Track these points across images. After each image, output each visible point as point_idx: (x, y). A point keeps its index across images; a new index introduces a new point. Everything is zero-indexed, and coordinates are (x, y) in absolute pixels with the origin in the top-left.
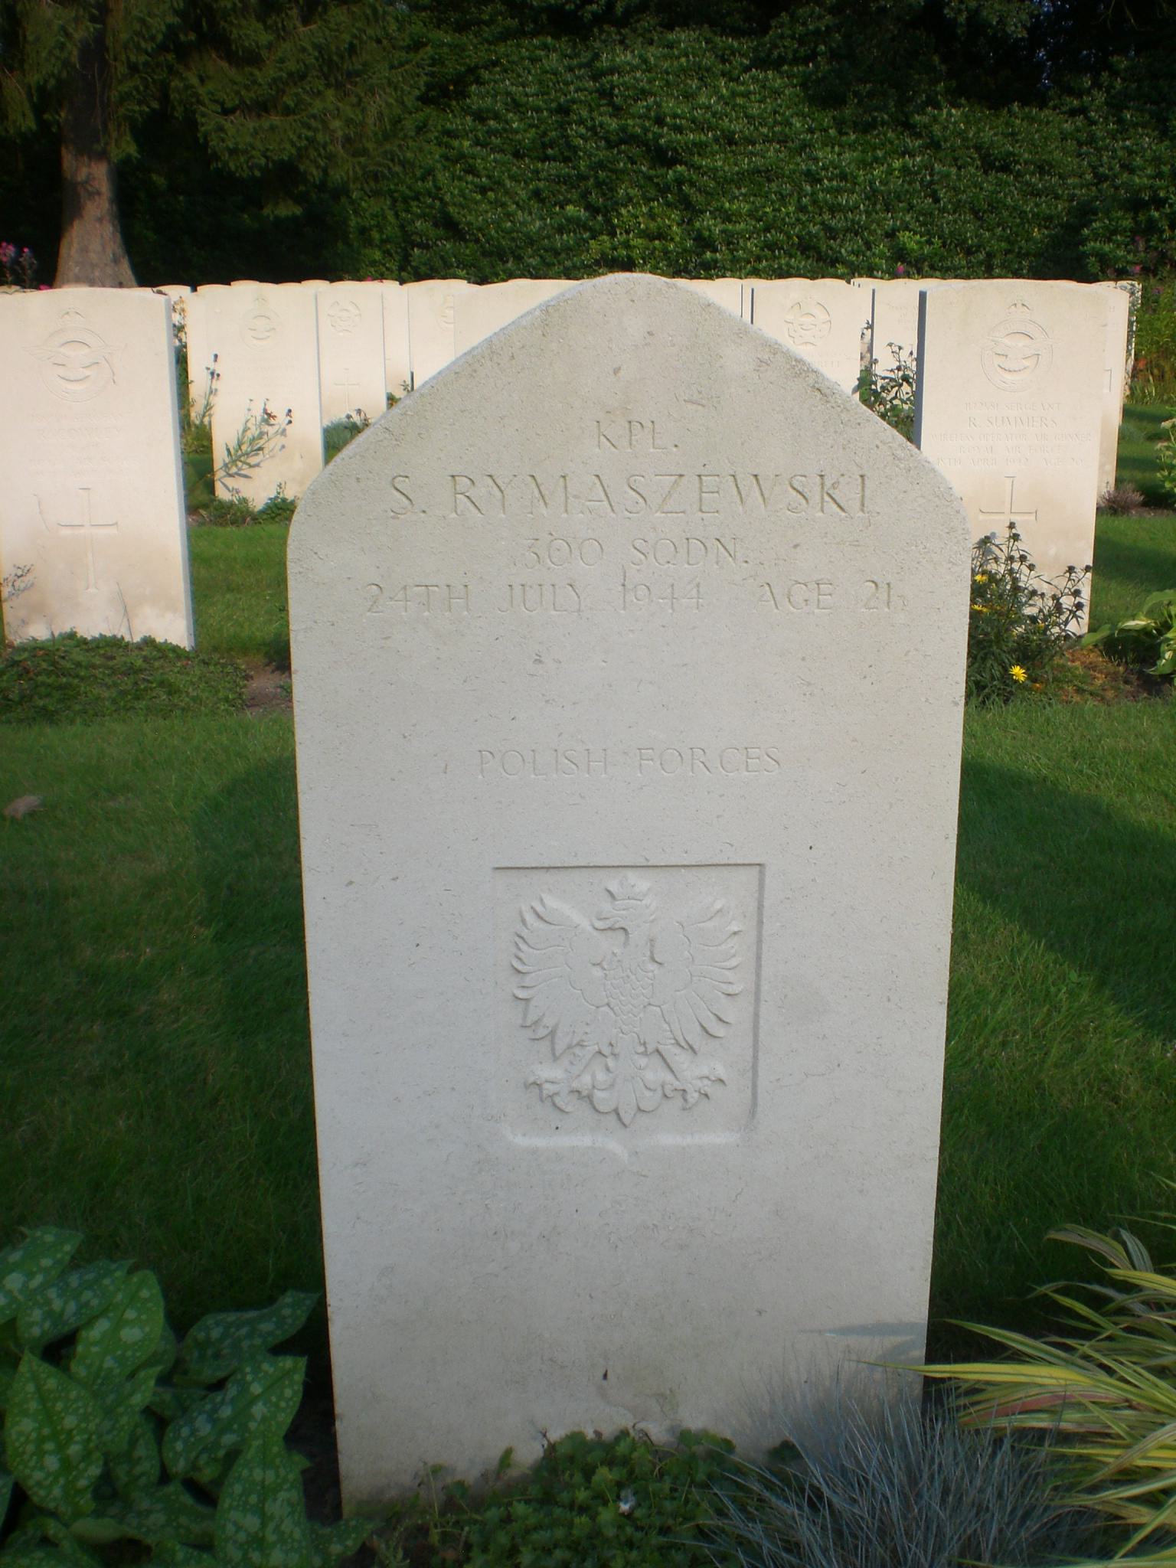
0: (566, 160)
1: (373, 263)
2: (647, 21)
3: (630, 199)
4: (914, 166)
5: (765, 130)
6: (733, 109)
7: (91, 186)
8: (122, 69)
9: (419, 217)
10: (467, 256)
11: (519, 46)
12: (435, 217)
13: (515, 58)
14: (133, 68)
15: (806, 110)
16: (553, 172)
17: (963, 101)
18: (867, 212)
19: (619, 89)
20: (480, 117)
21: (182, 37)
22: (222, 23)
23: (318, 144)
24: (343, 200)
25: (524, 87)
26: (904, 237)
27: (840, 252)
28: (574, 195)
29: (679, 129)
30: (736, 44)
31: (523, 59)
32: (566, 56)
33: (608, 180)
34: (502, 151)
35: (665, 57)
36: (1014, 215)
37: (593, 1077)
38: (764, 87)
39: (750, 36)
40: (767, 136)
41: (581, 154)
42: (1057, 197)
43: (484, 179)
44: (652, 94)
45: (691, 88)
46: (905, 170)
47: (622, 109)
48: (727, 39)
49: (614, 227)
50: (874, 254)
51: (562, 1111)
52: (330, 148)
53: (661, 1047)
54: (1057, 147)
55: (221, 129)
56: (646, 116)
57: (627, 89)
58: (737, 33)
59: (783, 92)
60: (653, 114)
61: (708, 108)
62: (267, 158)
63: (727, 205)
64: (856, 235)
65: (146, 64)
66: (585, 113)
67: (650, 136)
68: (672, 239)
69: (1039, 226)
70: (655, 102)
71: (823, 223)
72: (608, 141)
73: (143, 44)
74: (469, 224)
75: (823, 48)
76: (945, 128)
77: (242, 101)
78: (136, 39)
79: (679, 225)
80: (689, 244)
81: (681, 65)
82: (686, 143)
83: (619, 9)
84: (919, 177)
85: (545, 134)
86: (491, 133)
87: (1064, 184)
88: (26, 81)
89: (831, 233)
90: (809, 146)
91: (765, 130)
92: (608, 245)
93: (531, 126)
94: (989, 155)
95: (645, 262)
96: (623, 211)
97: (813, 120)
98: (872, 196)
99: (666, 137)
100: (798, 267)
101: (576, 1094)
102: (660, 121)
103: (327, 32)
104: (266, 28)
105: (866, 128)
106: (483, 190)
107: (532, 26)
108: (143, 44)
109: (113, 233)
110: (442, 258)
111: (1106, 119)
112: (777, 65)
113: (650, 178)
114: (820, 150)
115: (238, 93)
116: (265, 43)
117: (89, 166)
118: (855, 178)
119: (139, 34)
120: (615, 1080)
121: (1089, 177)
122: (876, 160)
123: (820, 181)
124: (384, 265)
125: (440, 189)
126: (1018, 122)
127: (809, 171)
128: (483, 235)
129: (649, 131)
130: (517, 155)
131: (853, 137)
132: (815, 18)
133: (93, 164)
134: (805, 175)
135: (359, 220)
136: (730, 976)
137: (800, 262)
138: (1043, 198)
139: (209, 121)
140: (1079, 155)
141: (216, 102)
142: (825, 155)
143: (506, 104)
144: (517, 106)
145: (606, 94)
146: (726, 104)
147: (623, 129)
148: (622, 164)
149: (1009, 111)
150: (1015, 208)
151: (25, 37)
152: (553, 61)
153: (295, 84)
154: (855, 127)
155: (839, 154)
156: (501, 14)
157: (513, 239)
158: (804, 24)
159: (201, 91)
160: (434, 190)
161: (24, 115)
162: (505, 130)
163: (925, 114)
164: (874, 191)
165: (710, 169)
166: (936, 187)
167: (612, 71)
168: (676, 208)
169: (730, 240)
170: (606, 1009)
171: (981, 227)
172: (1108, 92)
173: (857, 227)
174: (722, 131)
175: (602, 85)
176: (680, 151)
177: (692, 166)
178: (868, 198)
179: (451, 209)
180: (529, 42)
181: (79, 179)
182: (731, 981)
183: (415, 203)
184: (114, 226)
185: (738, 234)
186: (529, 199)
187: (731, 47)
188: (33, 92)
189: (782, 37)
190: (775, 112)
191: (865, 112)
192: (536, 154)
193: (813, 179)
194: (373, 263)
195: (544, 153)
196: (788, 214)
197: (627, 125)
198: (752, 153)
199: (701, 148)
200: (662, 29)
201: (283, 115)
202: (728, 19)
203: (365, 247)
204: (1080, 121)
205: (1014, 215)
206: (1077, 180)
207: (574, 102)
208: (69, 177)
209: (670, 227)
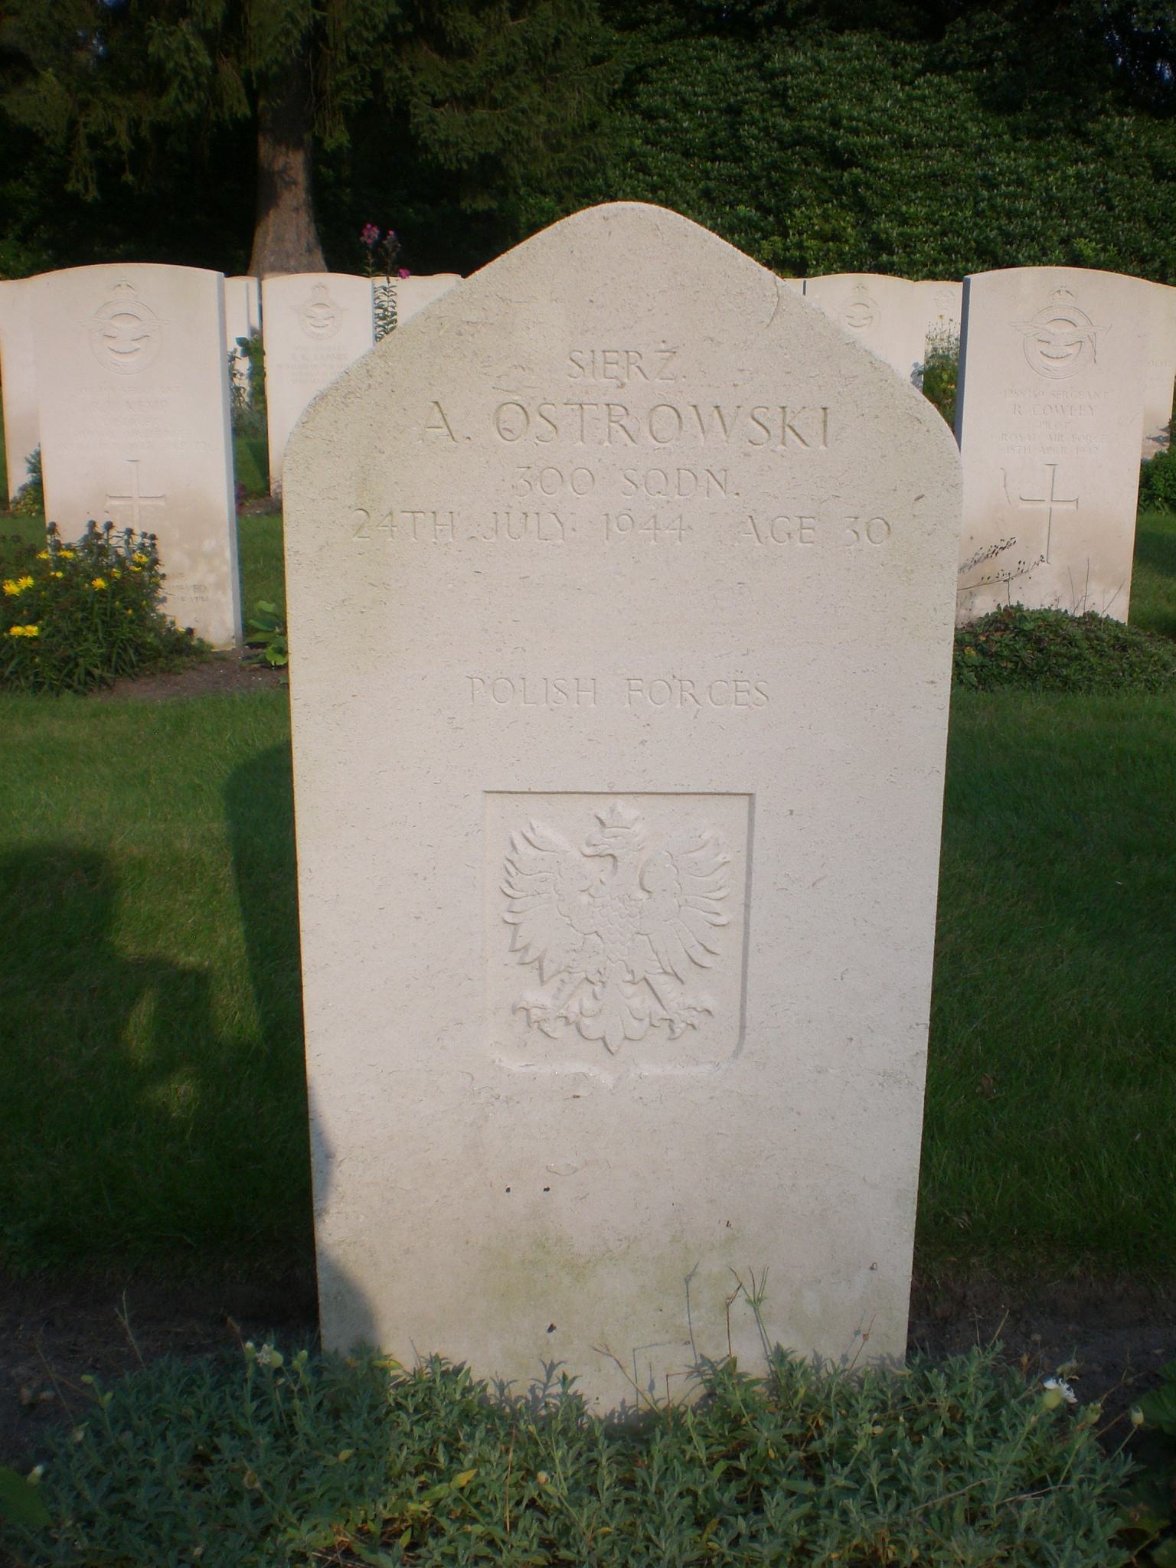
0: (737, 160)
3: (803, 201)
4: (1087, 173)
5: (941, 134)
6: (909, 113)
13: (682, 57)
14: (353, 58)
15: (981, 115)
18: (1043, 218)
19: (793, 90)
20: (649, 115)
21: (400, 29)
23: (523, 137)
25: (693, 87)
28: (745, 195)
29: (856, 132)
30: (908, 48)
32: (733, 56)
34: (672, 150)
35: (838, 60)
38: (938, 92)
40: (943, 141)
43: (655, 178)
44: (827, 96)
45: (864, 89)
46: (1078, 176)
48: (899, 44)
49: (786, 228)
53: (647, 976)
55: (432, 121)
57: (802, 90)
58: (910, 38)
60: (827, 115)
61: (884, 111)
63: (904, 208)
64: (1032, 241)
66: (757, 114)
67: (826, 137)
68: (847, 241)
71: (1000, 228)
72: (780, 142)
73: (365, 34)
75: (1000, 53)
76: (1120, 136)
77: (454, 95)
79: (853, 227)
80: (864, 246)
81: (854, 68)
83: (789, 12)
84: (1092, 184)
85: (714, 133)
86: (661, 131)
89: (1008, 238)
91: (941, 134)
92: (780, 245)
93: (701, 126)
95: (818, 263)
96: (797, 212)
98: (1048, 202)
102: (835, 124)
105: (1039, 135)
108: (365, 34)
112: (950, 70)
113: (824, 180)
115: (448, 85)
117: (287, 155)
122: (1050, 166)
125: (610, 186)
129: (824, 132)
130: (686, 154)
131: (1027, 143)
133: (290, 154)
139: (421, 112)
141: (427, 93)
142: (1001, 160)
143: (675, 103)
144: (686, 105)
145: (779, 95)
147: (798, 130)
148: (796, 166)
155: (1015, 160)
156: (668, 12)
158: (981, 29)
159: (416, 82)
160: (604, 188)
161: (240, 102)
162: (675, 130)
163: (1098, 121)
164: (1051, 198)
166: (1110, 194)
167: (784, 72)
168: (851, 210)
169: (907, 243)
173: (1033, 232)
175: (774, 87)
176: (857, 153)
177: (868, 168)
178: (1044, 204)
180: (696, 43)
182: (717, 911)
185: (917, 237)
186: (699, 198)
187: (904, 51)
188: (254, 78)
189: (958, 42)
193: (990, 183)
198: (928, 158)
199: (877, 149)
200: (831, 32)
201: (490, 108)
207: (745, 102)
208: (266, 166)
209: (845, 228)
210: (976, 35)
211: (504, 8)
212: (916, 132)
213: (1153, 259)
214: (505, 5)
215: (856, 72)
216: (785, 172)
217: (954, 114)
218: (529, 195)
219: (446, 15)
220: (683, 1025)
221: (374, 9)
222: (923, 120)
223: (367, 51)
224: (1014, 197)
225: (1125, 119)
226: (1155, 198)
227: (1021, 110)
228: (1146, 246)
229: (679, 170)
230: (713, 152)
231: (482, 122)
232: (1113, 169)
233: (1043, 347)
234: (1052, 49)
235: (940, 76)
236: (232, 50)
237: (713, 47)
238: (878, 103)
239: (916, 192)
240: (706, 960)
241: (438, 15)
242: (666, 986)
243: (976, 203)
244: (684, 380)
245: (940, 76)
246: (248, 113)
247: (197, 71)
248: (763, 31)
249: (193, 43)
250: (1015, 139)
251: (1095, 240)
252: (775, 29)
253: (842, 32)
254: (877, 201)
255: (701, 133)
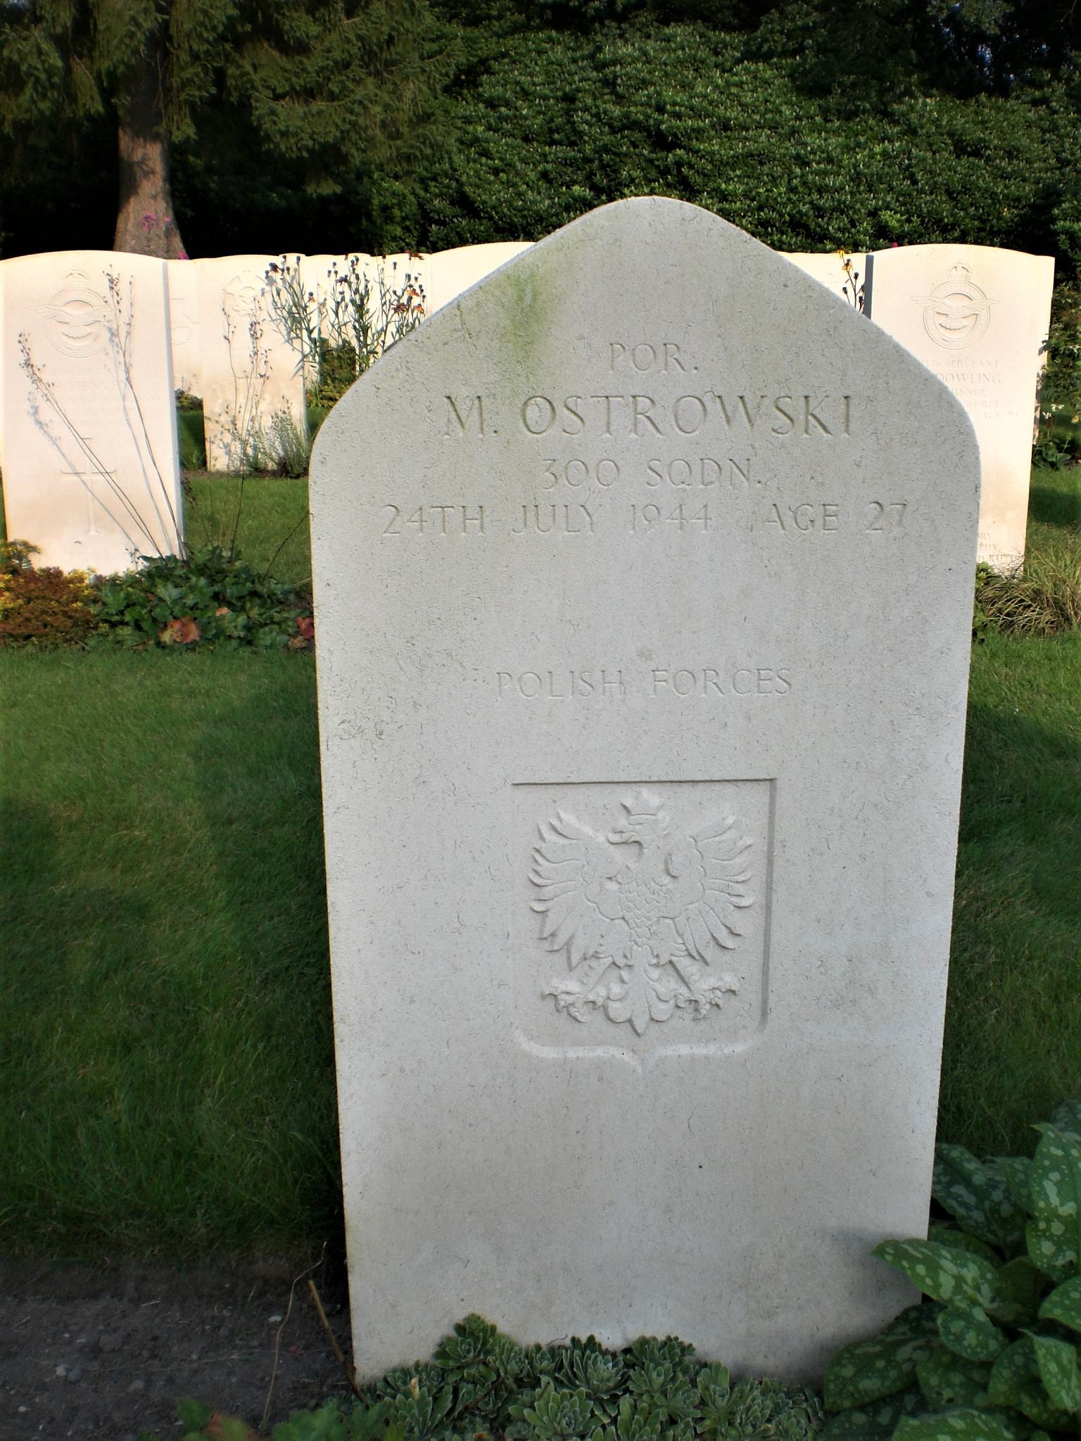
0: (572, 144)
1: (394, 239)
2: (644, 17)
3: (633, 180)
4: (893, 151)
5: (757, 117)
6: (728, 98)
7: (147, 166)
8: (185, 57)
9: (437, 196)
10: (483, 232)
11: (525, 39)
12: (451, 196)
14: (195, 57)
16: (560, 155)
17: (934, 91)
18: (852, 193)
20: (492, 104)
21: (239, 28)
22: (276, 15)
23: (360, 127)
24: (365, 180)
25: (532, 77)
26: (886, 216)
27: (828, 230)
28: (580, 176)
29: (678, 116)
30: (728, 38)
31: (530, 51)
32: (569, 48)
33: (612, 163)
34: (513, 136)
35: (663, 50)
36: (986, 196)
37: (609, 989)
38: (755, 77)
39: (740, 31)
40: (759, 123)
41: (587, 138)
42: (1024, 180)
43: (497, 162)
45: (687, 77)
46: (885, 154)
47: (624, 97)
48: (720, 34)
50: (859, 231)
51: (575, 1019)
52: (370, 132)
53: (674, 959)
54: (1023, 134)
55: (273, 113)
56: (647, 104)
57: (630, 78)
58: (728, 28)
59: (773, 83)
60: (653, 101)
61: (705, 96)
62: (314, 140)
63: (723, 186)
65: (207, 52)
66: (589, 101)
67: (651, 122)
69: (1009, 206)
70: (656, 92)
71: (811, 203)
72: (611, 127)
74: (484, 202)
75: (811, 42)
76: (922, 116)
77: (293, 88)
78: (199, 29)
81: (678, 57)
82: (685, 129)
83: (619, 7)
85: (552, 120)
86: (502, 118)
87: (1031, 167)
88: (95, 68)
89: (819, 211)
90: (798, 132)
91: (757, 117)
93: (539, 113)
94: (962, 141)
97: (801, 108)
98: (857, 178)
99: (667, 123)
100: (789, 243)
101: (591, 1005)
102: (660, 109)
103: (370, 25)
104: (315, 20)
105: (849, 116)
106: (496, 172)
107: (538, 21)
108: (205, 35)
109: (166, 209)
110: (458, 233)
111: (1066, 108)
112: (766, 58)
113: (651, 161)
114: (807, 135)
115: (288, 80)
116: (315, 34)
117: (145, 147)
118: (841, 161)
119: (202, 24)
120: (627, 994)
121: (1053, 161)
122: (858, 145)
123: (808, 164)
124: (404, 240)
125: (456, 170)
126: (987, 111)
127: (798, 155)
128: (497, 213)
129: (650, 117)
130: (526, 139)
132: (803, 15)
133: (148, 146)
134: (795, 159)
135: (382, 198)
136: (740, 889)
137: (791, 238)
138: (1012, 181)
139: (262, 105)
140: (1043, 142)
141: (268, 87)
142: (813, 141)
143: (516, 93)
144: (525, 94)
145: (610, 83)
146: (722, 93)
147: (627, 116)
149: (977, 101)
150: (986, 190)
151: (95, 25)
152: (558, 53)
153: (340, 73)
154: (839, 114)
155: (825, 140)
156: (509, 9)
157: (524, 217)
158: (793, 20)
159: (256, 78)
160: (450, 172)
161: (92, 98)
162: (515, 116)
163: (902, 103)
164: (858, 174)
165: (707, 153)
166: (913, 170)
168: (675, 188)
170: (621, 922)
171: (955, 206)
172: (1067, 83)
174: (719, 118)
175: (605, 76)
177: (691, 150)
178: (852, 180)
179: (467, 189)
181: (136, 160)
182: (740, 893)
183: (433, 183)
184: (167, 203)
185: (735, 212)
186: (538, 180)
187: (724, 42)
188: (104, 77)
190: (766, 101)
191: (849, 101)
192: (543, 139)
193: (803, 162)
194: (394, 239)
195: (551, 137)
196: (780, 194)
197: (630, 112)
198: (746, 139)
199: (699, 131)
201: (328, 101)
202: (719, 16)
203: (387, 224)
204: (1042, 110)
205: (986, 196)
206: (1042, 165)
207: (578, 90)
208: (126, 157)
210: (789, 25)
211: (339, 8)
212: (733, 115)
213: (953, 228)
214: (340, 5)
215: (680, 62)
216: (615, 154)
217: (769, 98)
218: (382, 179)
219: (284, 15)
220: (708, 1007)
221: (213, 12)
222: (741, 104)
223: (208, 51)
224: (825, 173)
225: (928, 100)
226: (955, 172)
227: (831, 93)
228: (947, 217)
229: (519, 154)
230: (551, 137)
231: (320, 113)
232: (917, 146)
233: (942, 320)
234: (858, 37)
235: (756, 63)
236: (85, 52)
237: (550, 40)
238: (699, 89)
239: (734, 171)
240: (729, 943)
241: (276, 15)
242: (690, 968)
243: (790, 181)
244: (695, 371)
245: (756, 63)
246: (101, 110)
247: (50, 72)
248: (597, 25)
249: (44, 46)
250: (826, 120)
251: (900, 212)
252: (607, 22)
253: (668, 25)
254: (699, 180)
255: (540, 120)
